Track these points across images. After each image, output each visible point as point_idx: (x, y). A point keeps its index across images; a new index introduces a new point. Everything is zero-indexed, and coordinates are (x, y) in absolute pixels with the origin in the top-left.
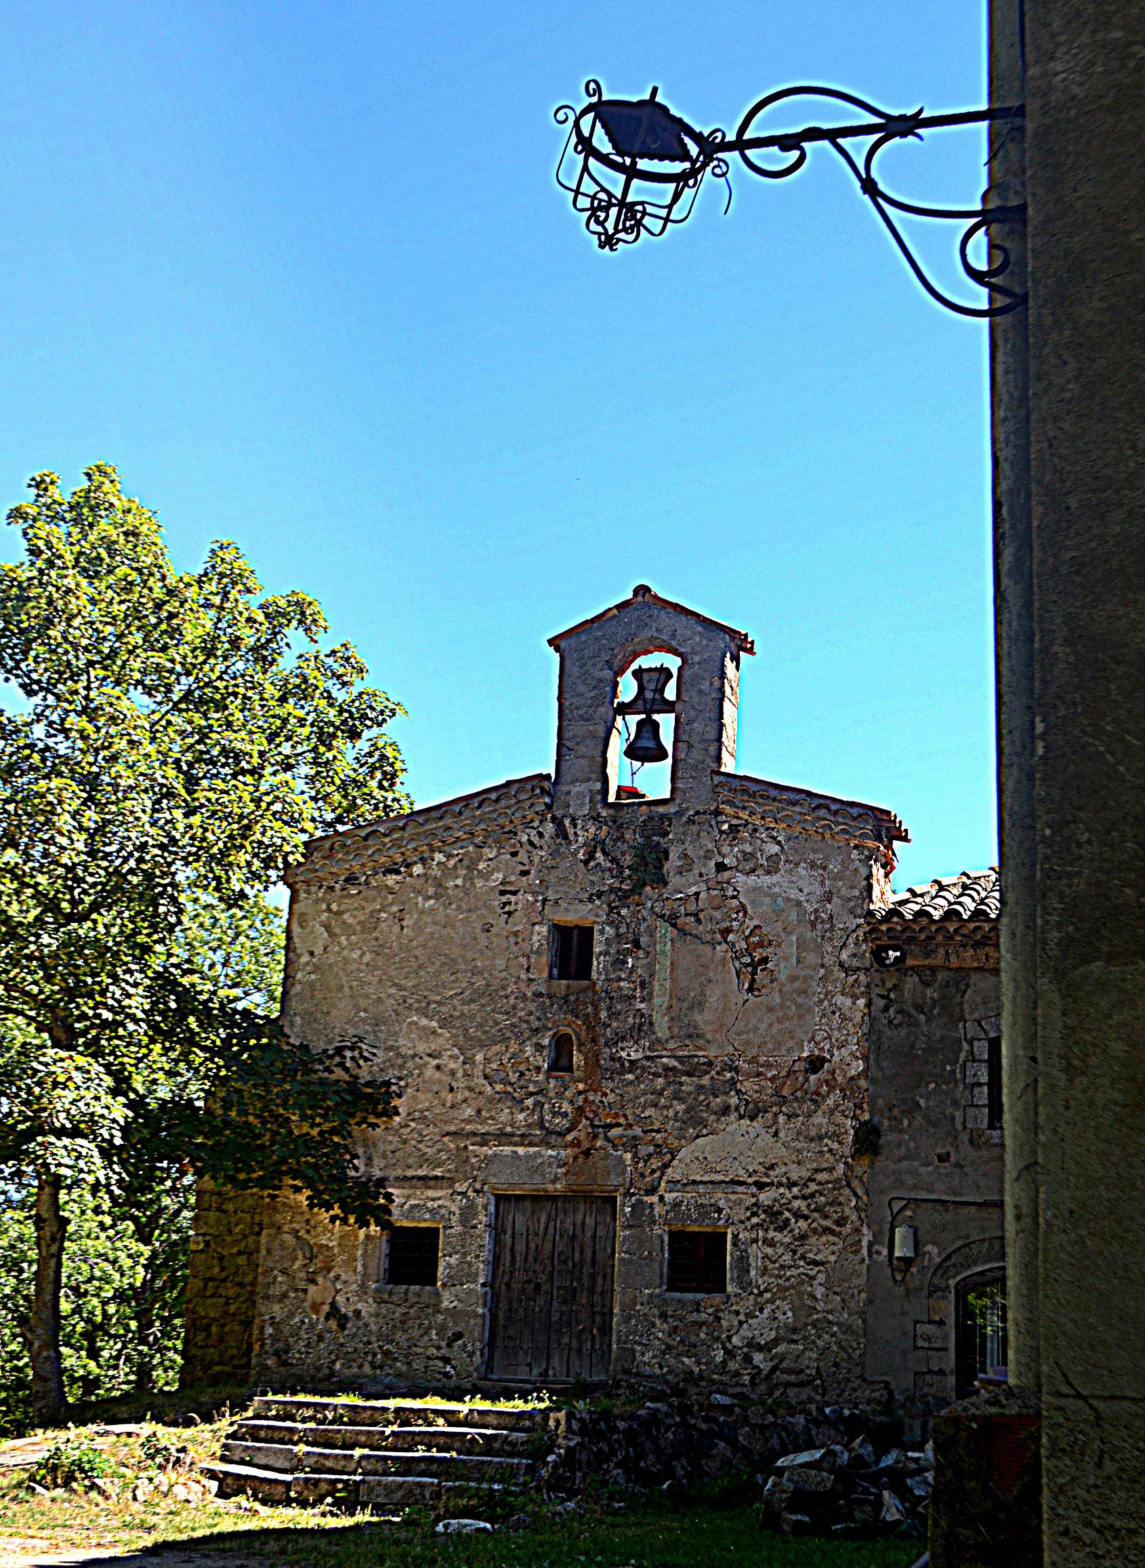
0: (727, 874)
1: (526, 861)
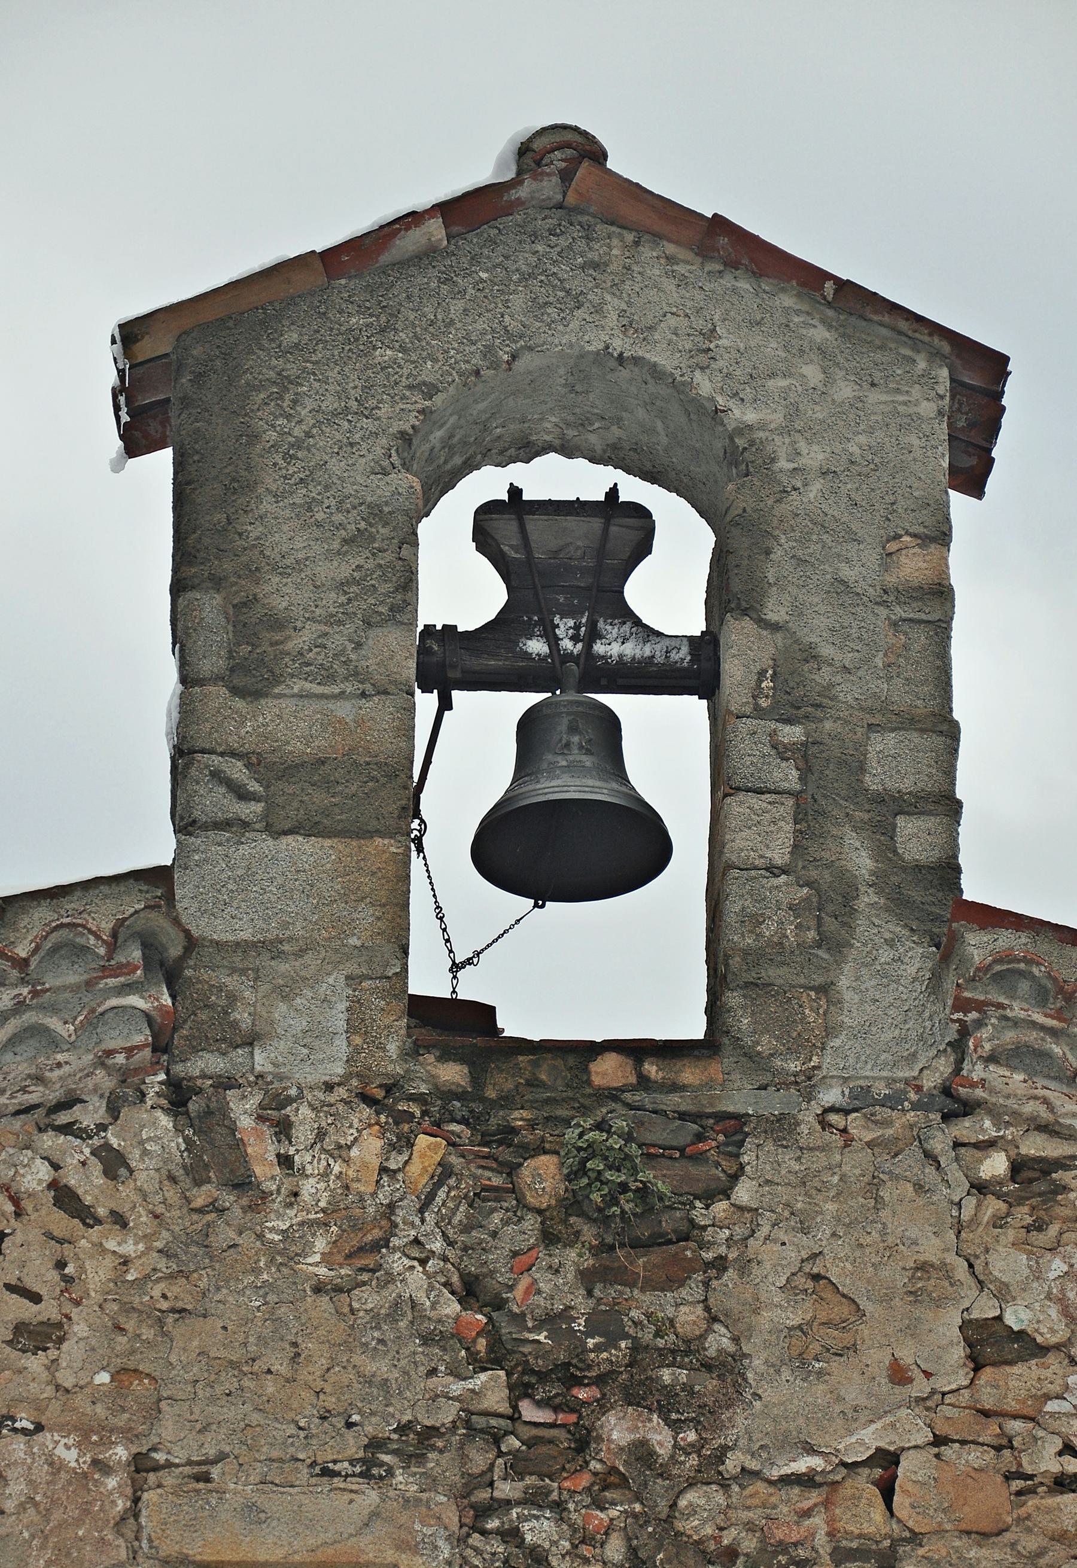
0: (1018, 1380)
1: (42, 1276)
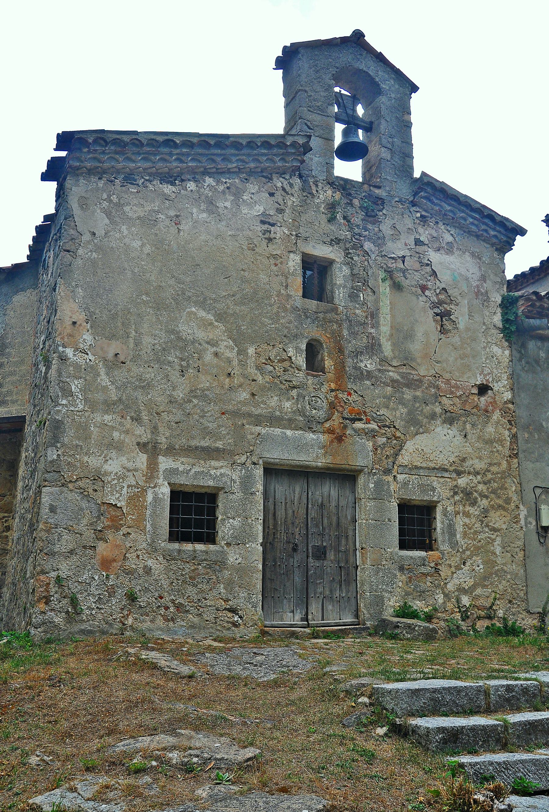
0: (420, 249)
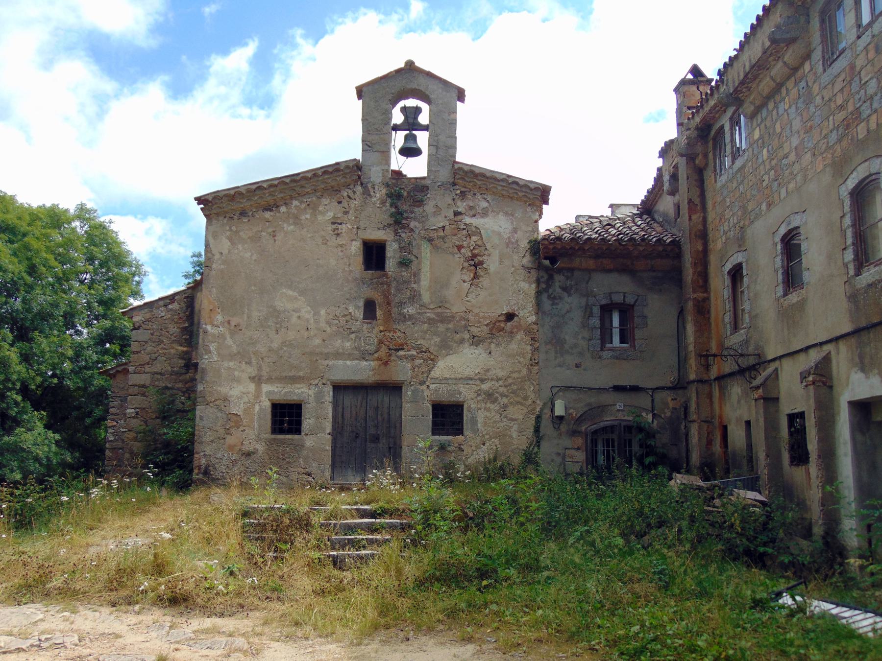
0: (459, 217)
1: (346, 206)
